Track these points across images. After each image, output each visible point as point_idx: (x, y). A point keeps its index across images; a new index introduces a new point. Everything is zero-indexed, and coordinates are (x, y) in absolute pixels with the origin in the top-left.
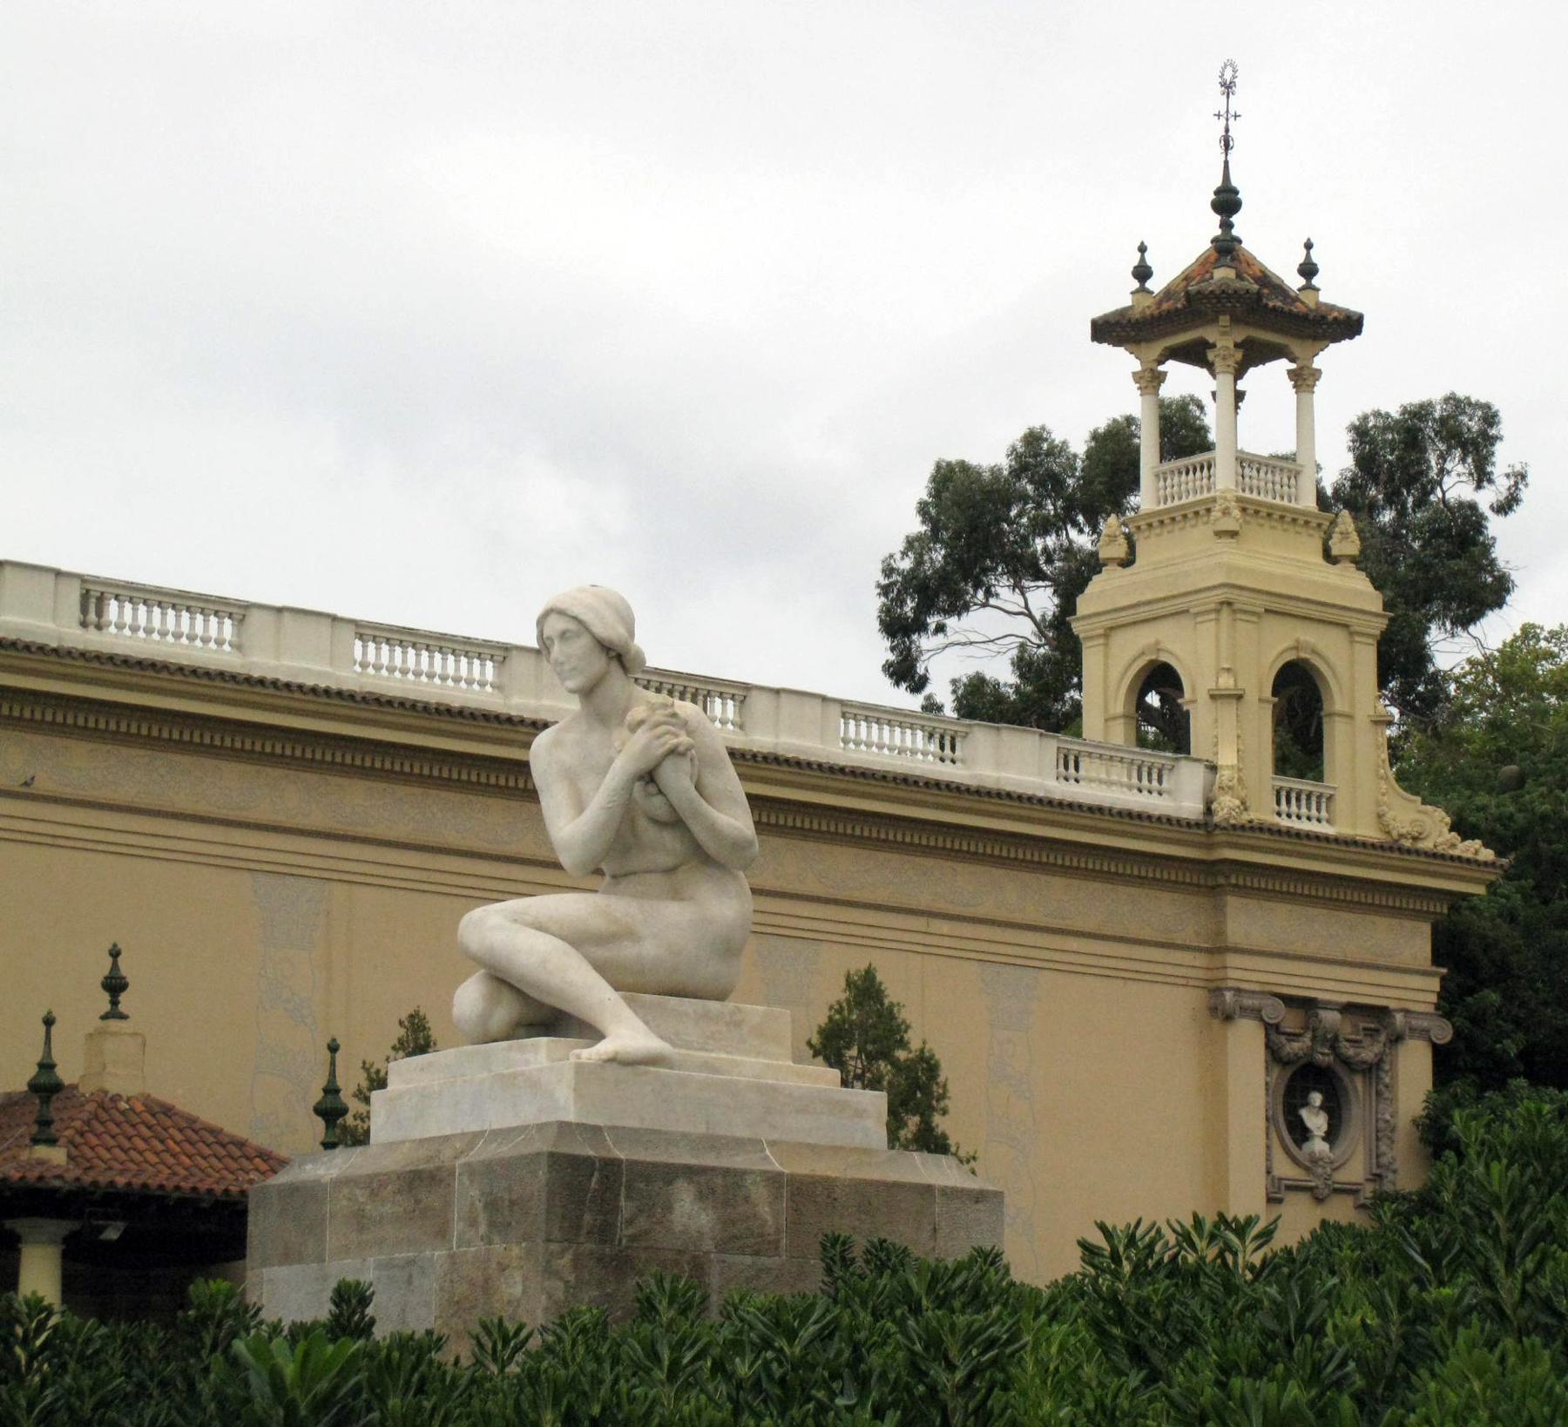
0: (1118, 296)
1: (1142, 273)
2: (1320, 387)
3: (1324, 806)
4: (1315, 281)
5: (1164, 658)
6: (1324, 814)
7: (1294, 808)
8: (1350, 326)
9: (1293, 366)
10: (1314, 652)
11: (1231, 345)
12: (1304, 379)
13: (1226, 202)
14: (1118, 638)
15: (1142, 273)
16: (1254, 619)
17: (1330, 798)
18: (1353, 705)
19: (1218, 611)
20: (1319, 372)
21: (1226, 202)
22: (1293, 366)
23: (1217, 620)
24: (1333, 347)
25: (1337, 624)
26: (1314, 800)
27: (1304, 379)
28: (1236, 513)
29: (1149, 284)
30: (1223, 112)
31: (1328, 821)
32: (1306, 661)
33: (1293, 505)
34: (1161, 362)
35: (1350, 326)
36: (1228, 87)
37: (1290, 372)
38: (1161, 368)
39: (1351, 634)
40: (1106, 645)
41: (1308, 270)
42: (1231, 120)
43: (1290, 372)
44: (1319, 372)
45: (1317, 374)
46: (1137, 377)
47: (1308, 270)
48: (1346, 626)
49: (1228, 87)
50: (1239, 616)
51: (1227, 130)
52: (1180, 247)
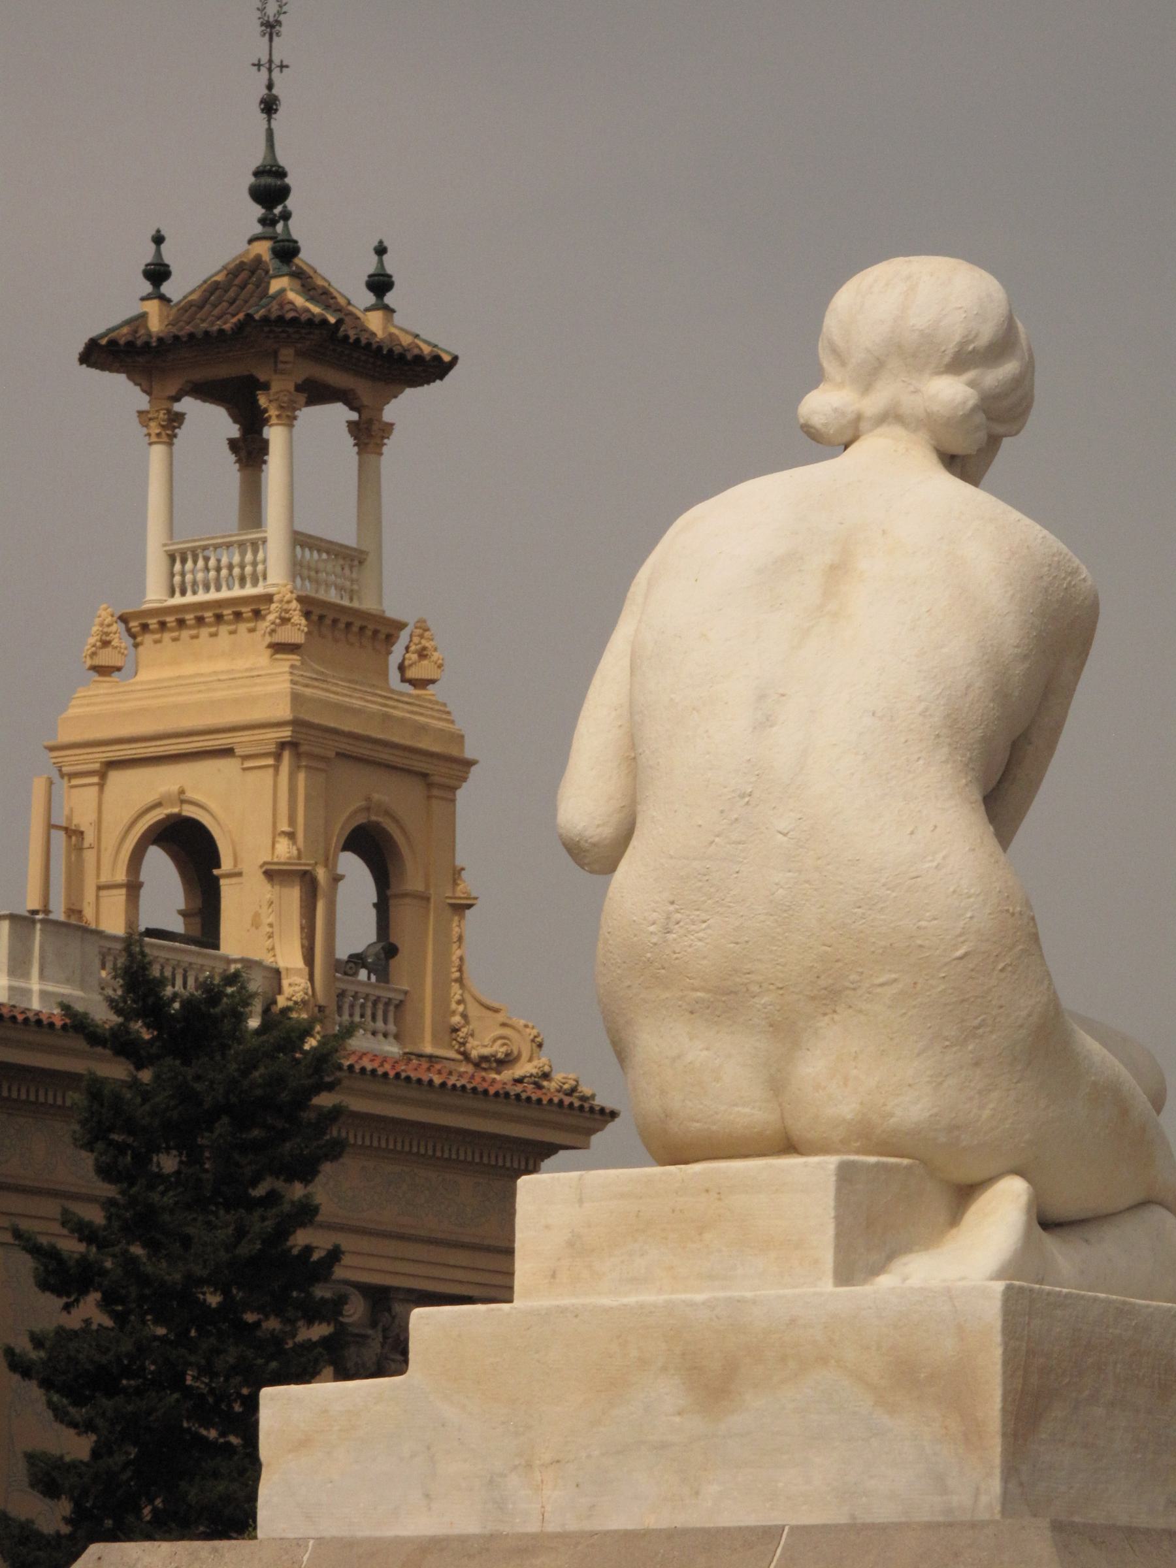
0: (121, 302)
1: (157, 274)
2: (391, 447)
3: (391, 1015)
4: (389, 299)
5: (189, 811)
6: (392, 1028)
7: (380, 1024)
8: (429, 368)
9: (354, 416)
10: (387, 813)
11: (292, 388)
12: (368, 435)
13: (270, 190)
14: (116, 778)
15: (157, 274)
16: (322, 765)
17: (399, 1005)
18: (427, 886)
19: (278, 756)
20: (390, 427)
21: (270, 190)
22: (354, 416)
23: (276, 768)
24: (409, 391)
25: (409, 772)
26: (381, 1006)
27: (368, 435)
28: (297, 618)
29: (166, 288)
30: (265, 60)
31: (397, 1037)
32: (377, 825)
33: (356, 604)
34: (177, 399)
35: (429, 368)
36: (271, 27)
37: (351, 424)
38: (178, 407)
39: (430, 786)
40: (101, 786)
41: (380, 285)
42: (276, 73)
43: (351, 424)
44: (390, 427)
45: (387, 429)
46: (233, 445)
47: (380, 285)
48: (425, 776)
49: (271, 27)
50: (435, 792)
51: (270, 86)
52: (213, 239)
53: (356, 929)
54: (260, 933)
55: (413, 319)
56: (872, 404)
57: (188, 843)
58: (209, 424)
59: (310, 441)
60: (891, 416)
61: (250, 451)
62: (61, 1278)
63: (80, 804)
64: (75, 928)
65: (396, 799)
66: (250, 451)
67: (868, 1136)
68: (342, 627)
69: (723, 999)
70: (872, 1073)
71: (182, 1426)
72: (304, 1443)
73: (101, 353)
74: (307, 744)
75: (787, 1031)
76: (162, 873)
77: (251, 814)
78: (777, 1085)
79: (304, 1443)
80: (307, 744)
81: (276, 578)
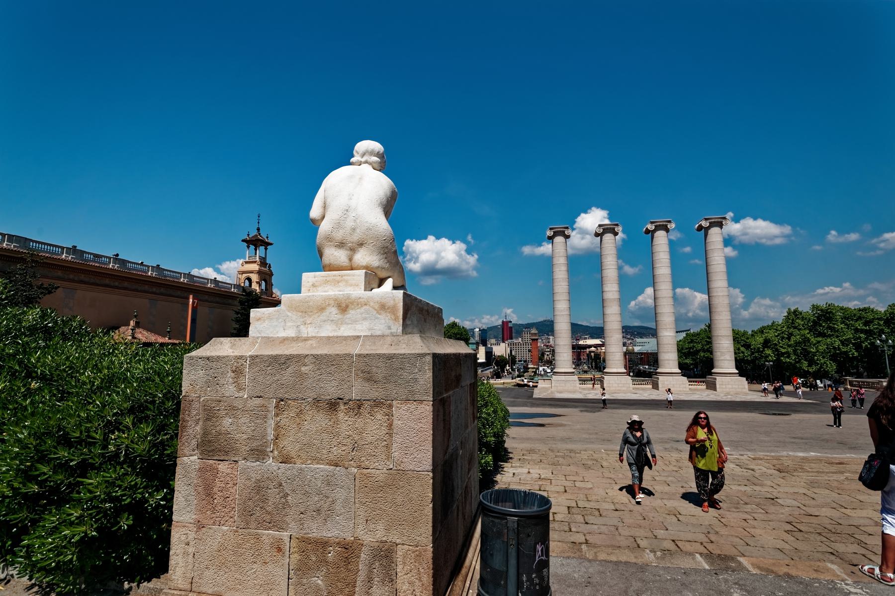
0: (246, 237)
8: (271, 244)
12: (266, 249)
13: (258, 229)
21: (258, 229)
27: (266, 249)
35: (271, 244)
52: (253, 233)
53: (263, 287)
54: (255, 286)
55: (270, 241)
56: (363, 160)
57: (249, 279)
58: (252, 247)
59: (261, 251)
60: (366, 162)
61: (256, 250)
62: (237, 313)
63: (240, 276)
64: (239, 285)
65: (267, 277)
66: (256, 250)
67: (366, 268)
68: (263, 262)
69: (341, 245)
70: (366, 257)
71: (834, 230)
72: (259, 319)
73: (243, 241)
74: (259, 272)
75: (353, 250)
76: (247, 281)
77: (255, 278)
78: (351, 260)
79: (259, 319)
80: (259, 272)
81: (258, 259)
